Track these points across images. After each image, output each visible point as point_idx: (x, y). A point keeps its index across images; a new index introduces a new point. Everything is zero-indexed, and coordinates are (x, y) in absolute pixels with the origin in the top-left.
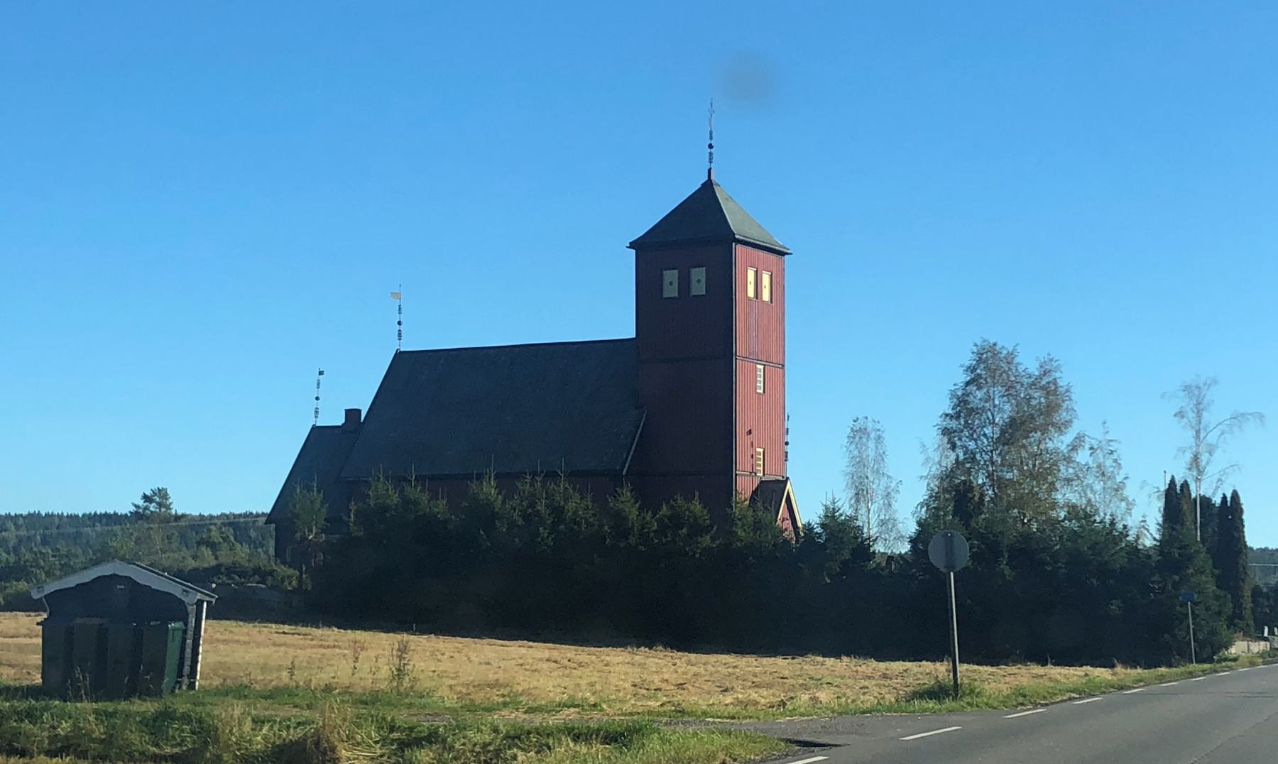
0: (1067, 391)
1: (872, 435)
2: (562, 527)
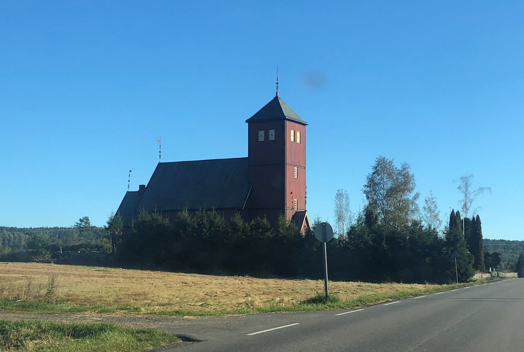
0: (413, 176)
1: (344, 196)
2: (213, 229)
